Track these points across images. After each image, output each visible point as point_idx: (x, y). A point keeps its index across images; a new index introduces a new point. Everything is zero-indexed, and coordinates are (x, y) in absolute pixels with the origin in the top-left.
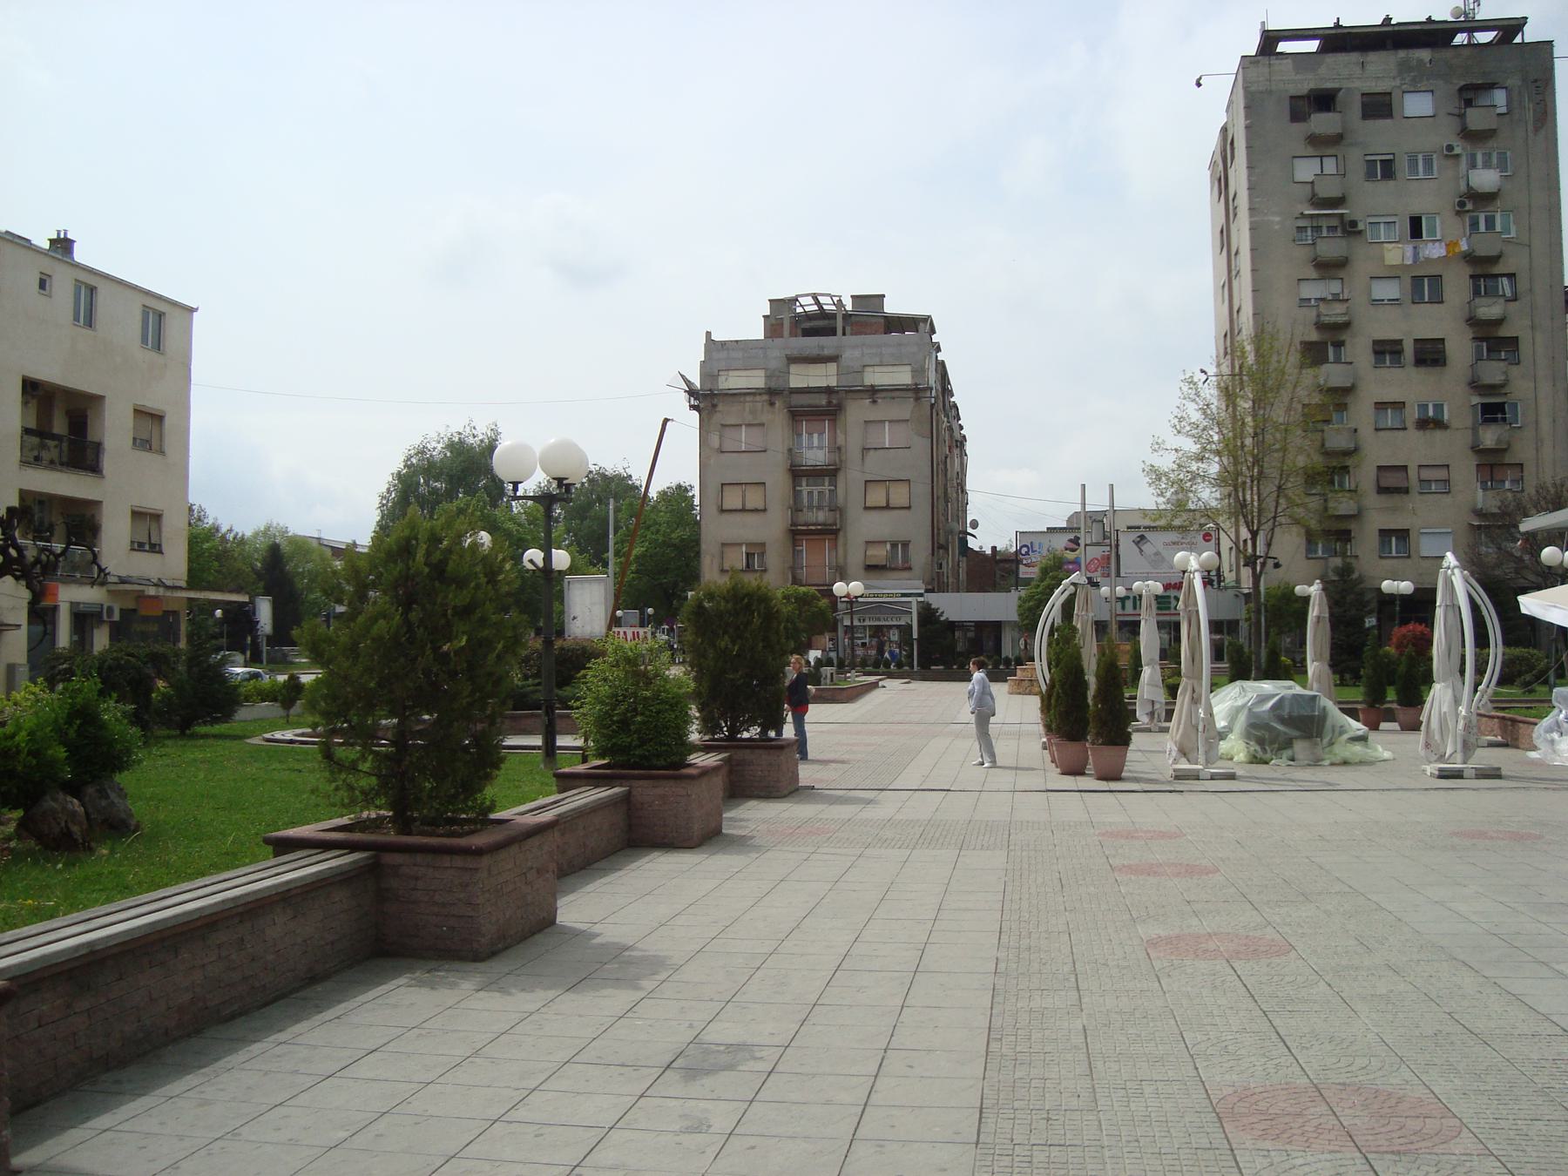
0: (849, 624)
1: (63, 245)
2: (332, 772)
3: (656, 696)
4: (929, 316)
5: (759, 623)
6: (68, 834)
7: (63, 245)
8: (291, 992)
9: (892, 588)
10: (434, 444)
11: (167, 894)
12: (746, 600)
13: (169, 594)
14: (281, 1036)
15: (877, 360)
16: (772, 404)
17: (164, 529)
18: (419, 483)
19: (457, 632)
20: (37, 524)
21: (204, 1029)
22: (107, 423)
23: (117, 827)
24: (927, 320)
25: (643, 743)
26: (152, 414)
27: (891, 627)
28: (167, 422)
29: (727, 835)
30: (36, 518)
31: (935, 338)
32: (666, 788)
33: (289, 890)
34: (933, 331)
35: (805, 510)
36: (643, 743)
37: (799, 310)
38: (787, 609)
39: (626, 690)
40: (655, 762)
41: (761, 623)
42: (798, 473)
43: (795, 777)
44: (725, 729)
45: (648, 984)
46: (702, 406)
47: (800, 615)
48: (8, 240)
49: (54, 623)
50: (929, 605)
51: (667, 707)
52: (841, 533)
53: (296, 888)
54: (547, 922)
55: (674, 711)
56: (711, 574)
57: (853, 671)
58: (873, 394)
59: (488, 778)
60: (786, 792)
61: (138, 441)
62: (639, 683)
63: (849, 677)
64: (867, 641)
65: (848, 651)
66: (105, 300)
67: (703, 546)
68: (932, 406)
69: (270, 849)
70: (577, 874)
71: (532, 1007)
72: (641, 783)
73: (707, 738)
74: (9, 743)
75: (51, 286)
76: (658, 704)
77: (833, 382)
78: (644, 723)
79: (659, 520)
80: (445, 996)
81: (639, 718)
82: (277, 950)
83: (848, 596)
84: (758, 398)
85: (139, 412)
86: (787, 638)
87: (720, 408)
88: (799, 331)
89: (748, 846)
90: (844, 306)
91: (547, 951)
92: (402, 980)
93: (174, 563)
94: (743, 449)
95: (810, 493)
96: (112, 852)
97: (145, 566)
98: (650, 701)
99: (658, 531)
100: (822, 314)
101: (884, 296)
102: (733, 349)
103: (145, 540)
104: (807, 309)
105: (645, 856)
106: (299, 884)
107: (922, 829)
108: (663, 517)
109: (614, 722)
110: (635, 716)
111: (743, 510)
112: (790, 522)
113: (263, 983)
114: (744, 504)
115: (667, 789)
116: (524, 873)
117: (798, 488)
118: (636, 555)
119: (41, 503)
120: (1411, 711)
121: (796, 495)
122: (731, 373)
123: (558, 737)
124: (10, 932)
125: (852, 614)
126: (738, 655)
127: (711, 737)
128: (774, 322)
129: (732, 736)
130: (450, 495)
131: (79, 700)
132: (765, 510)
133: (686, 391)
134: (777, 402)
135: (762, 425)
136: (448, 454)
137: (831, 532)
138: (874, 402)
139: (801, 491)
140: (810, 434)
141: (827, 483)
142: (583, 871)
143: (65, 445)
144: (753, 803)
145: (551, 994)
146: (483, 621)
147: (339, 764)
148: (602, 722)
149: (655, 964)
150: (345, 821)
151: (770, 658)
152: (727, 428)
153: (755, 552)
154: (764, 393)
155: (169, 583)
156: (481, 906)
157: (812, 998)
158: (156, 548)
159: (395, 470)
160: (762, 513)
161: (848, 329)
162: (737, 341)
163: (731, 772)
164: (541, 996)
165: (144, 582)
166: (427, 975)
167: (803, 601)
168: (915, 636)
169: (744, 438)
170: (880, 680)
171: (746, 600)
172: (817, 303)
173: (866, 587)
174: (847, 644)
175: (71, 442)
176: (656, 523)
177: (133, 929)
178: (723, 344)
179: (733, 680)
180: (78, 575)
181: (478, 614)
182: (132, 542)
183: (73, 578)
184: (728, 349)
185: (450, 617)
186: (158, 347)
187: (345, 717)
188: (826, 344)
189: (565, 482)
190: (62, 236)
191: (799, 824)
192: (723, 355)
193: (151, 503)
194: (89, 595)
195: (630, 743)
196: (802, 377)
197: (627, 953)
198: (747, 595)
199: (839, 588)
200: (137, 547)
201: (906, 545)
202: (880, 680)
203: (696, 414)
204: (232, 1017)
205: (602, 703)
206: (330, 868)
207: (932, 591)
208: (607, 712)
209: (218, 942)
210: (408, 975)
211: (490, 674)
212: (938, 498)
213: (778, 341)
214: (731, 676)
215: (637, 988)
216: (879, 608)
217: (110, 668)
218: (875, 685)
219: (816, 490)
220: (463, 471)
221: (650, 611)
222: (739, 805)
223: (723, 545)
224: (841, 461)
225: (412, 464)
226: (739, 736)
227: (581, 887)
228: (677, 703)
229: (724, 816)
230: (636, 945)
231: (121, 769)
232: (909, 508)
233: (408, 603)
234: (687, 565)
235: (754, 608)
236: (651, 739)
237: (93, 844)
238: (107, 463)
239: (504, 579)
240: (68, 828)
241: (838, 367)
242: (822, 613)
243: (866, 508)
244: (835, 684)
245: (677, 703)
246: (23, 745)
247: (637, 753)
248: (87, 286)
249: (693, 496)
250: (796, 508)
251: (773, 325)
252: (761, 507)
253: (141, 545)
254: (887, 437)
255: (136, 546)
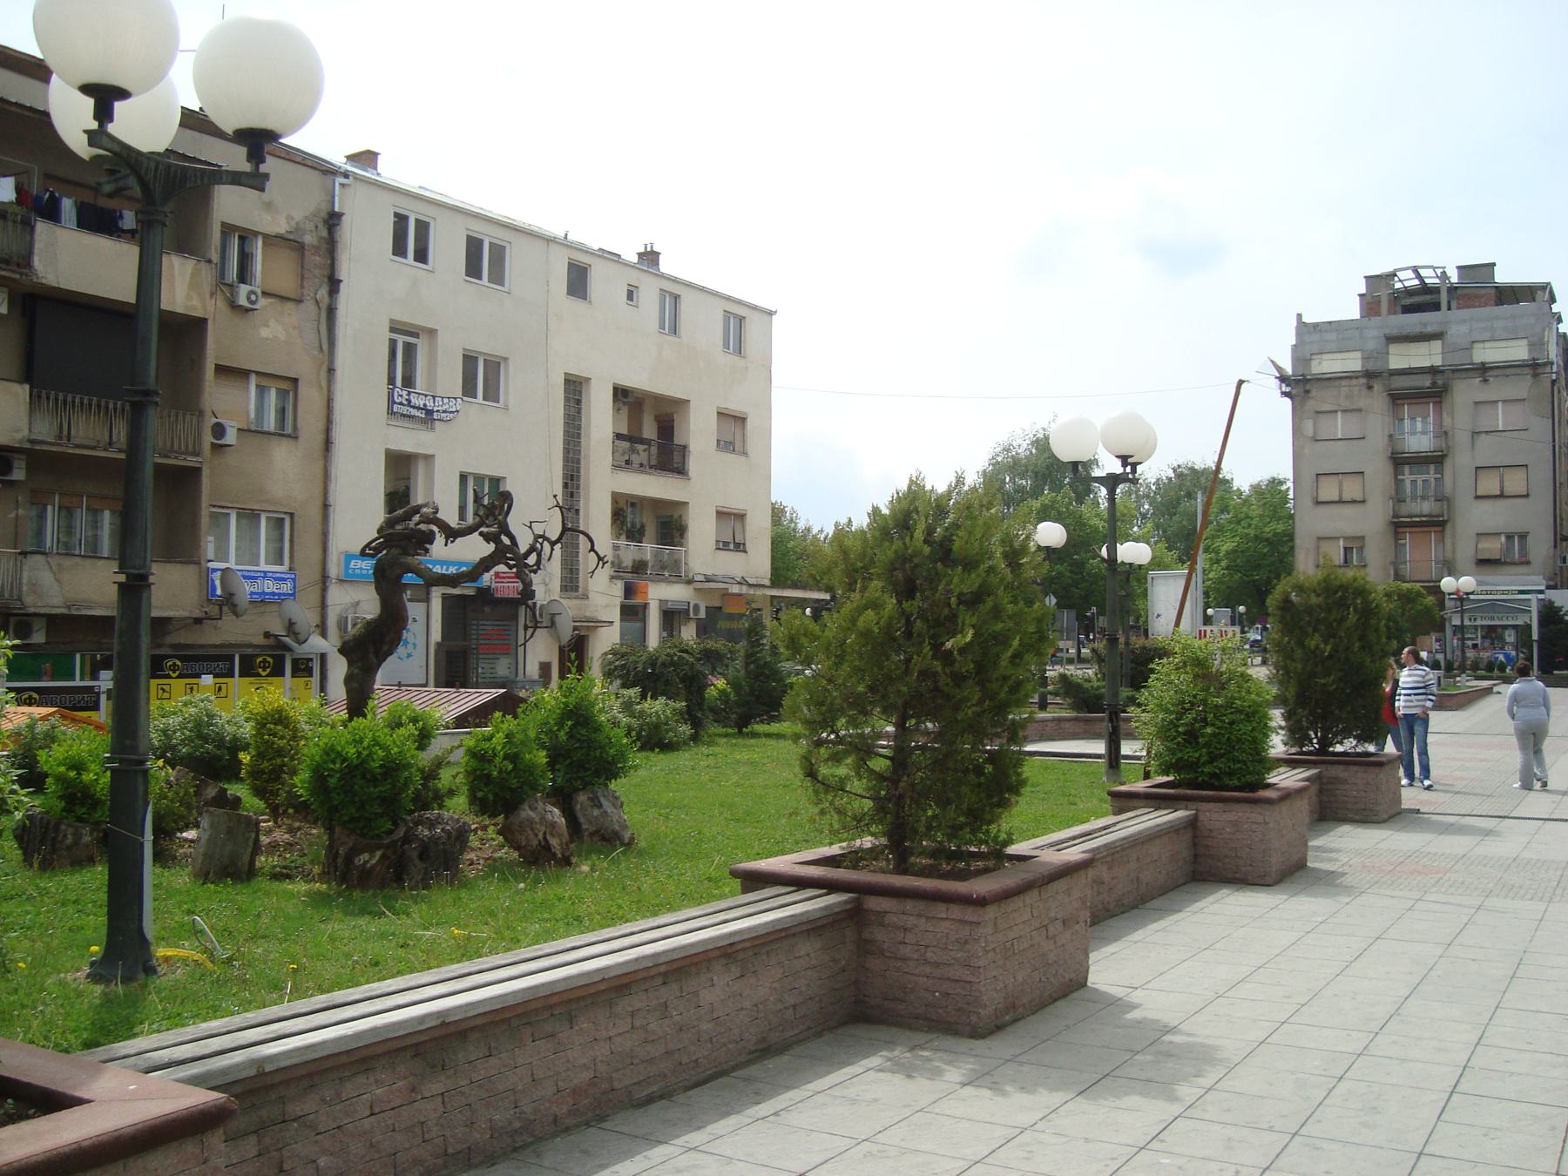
0: (1459, 623)
1: (650, 257)
2: (816, 792)
3: (1230, 704)
4: (1549, 284)
5: (1355, 620)
6: (547, 847)
7: (650, 257)
8: (734, 1068)
9: (1506, 584)
10: (1020, 441)
11: (578, 944)
12: (1340, 594)
13: (752, 592)
14: (695, 1138)
15: (1487, 335)
16: (1370, 388)
17: (748, 528)
18: (1004, 481)
19: (963, 624)
20: (629, 525)
21: (608, 1116)
22: (692, 426)
23: (610, 839)
24: (1546, 288)
25: (1213, 759)
26: (735, 417)
27: (1505, 627)
28: (749, 424)
29: (1313, 869)
30: (629, 519)
31: (1555, 308)
32: (1239, 813)
33: (731, 945)
34: (1553, 300)
35: (1408, 500)
36: (1213, 759)
37: (1398, 285)
38: (1388, 606)
39: (1195, 696)
40: (1226, 781)
41: (1358, 620)
42: (1399, 461)
43: (1398, 800)
44: (1315, 741)
45: (1187, 1092)
46: (1294, 392)
47: (1403, 614)
48: (600, 256)
49: (644, 621)
50: (1551, 603)
51: (1242, 717)
52: (1449, 526)
53: (744, 941)
54: (1077, 984)
55: (1250, 722)
56: (1306, 566)
57: (1464, 675)
58: (1484, 372)
59: (1004, 804)
60: (1386, 816)
61: (722, 443)
62: (1209, 688)
63: (1459, 682)
64: (1479, 642)
65: (1458, 653)
66: (688, 301)
67: (1298, 541)
68: (1553, 382)
69: (737, 884)
70: (1126, 915)
71: (1025, 1119)
72: (1211, 805)
73: (1293, 750)
74: (486, 745)
75: (638, 297)
76: (1232, 713)
77: (1437, 361)
78: (1214, 735)
79: (1251, 514)
80: (920, 1089)
81: (1209, 730)
82: (715, 1017)
83: (1457, 592)
84: (1354, 382)
85: (722, 415)
86: (1389, 638)
87: (1313, 393)
88: (1399, 309)
89: (1337, 885)
90: (1448, 278)
91: (1068, 1027)
92: (874, 1061)
93: (757, 563)
94: (1340, 437)
95: (1414, 482)
96: (593, 870)
97: (730, 565)
98: (1222, 710)
99: (1250, 525)
100: (1425, 289)
101: (1494, 264)
102: (1326, 331)
103: (730, 539)
104: (1407, 284)
105: (1211, 894)
106: (745, 937)
107: (1559, 873)
108: (1255, 511)
109: (1179, 733)
110: (1204, 727)
111: (1340, 502)
112: (1391, 513)
113: (694, 1058)
114: (1340, 496)
115: (1240, 814)
116: (1045, 926)
117: (1400, 477)
118: (1226, 552)
119: (633, 505)
120: (1517, 675)
121: (1398, 483)
122: (1324, 356)
123: (1123, 742)
124: (366, 986)
125: (1462, 612)
126: (1330, 656)
127: (1299, 749)
128: (1370, 300)
129: (1323, 749)
130: (1036, 492)
131: (572, 699)
132: (1364, 501)
133: (1277, 378)
134: (1375, 385)
135: (1359, 410)
136: (1034, 451)
137: (1437, 524)
138: (1485, 381)
139: (1403, 480)
140: (1413, 419)
141: (1432, 472)
142: (1135, 911)
143: (654, 450)
144: (1346, 828)
145: (1057, 1098)
146: (997, 613)
147: (824, 784)
148: (1166, 731)
149: (1201, 1057)
150: (836, 850)
151: (1369, 660)
152: (1321, 415)
153: (1353, 547)
154: (1362, 377)
155: (751, 581)
156: (981, 970)
157: (1416, 1142)
158: (740, 547)
159: (980, 469)
160: (1360, 505)
161: (1454, 304)
162: (1330, 322)
163: (1321, 792)
164: (1046, 1098)
165: (727, 580)
166: (908, 1055)
167: (1407, 598)
168: (1535, 636)
169: (1340, 426)
170: (1495, 685)
171: (1340, 594)
172: (1419, 276)
173: (1479, 583)
174: (1455, 645)
175: (660, 446)
176: (1248, 517)
177: (506, 995)
178: (1316, 325)
179: (1324, 685)
180: (667, 574)
181: (989, 603)
182: (717, 541)
183: (662, 577)
184: (1320, 331)
185: (954, 606)
186: (739, 351)
187: (832, 727)
188: (1428, 320)
189: (1130, 460)
190: (649, 249)
191: (1401, 859)
192: (1316, 337)
193: (736, 504)
194: (676, 593)
195: (1198, 759)
196: (1400, 359)
197: (1167, 1038)
198: (1341, 586)
199: (1447, 583)
200: (723, 546)
201: (1523, 537)
202: (1495, 685)
203: (1288, 401)
204: (650, 1100)
205: (1167, 711)
206: (792, 916)
207: (1554, 587)
208: (1171, 722)
209: (631, 1009)
210: (884, 1053)
211: (1005, 678)
212: (1561, 484)
213: (1376, 320)
214: (1322, 681)
215: (1172, 1098)
216: (1493, 606)
217: (663, 664)
218: (1488, 691)
219: (1420, 478)
220: (1048, 468)
221: (1242, 609)
222: (1330, 831)
223: (1319, 539)
224: (1448, 447)
225: (998, 463)
226: (1331, 749)
227: (1126, 936)
228: (1254, 713)
229: (1310, 844)
230: (1180, 1027)
231: (615, 776)
232: (1527, 496)
233: (907, 590)
234: (1281, 561)
235: (1349, 602)
236: (1224, 754)
237: (574, 860)
238: (693, 465)
239: (1029, 563)
240: (545, 838)
241: (1443, 344)
242: (1428, 610)
243: (1477, 497)
244: (1443, 690)
245: (1254, 713)
246: (499, 748)
247: (1206, 770)
248: (671, 294)
249: (1289, 488)
250: (1399, 499)
251: (1370, 304)
252: (1359, 497)
253: (726, 544)
254: (1501, 418)
255: (721, 546)
